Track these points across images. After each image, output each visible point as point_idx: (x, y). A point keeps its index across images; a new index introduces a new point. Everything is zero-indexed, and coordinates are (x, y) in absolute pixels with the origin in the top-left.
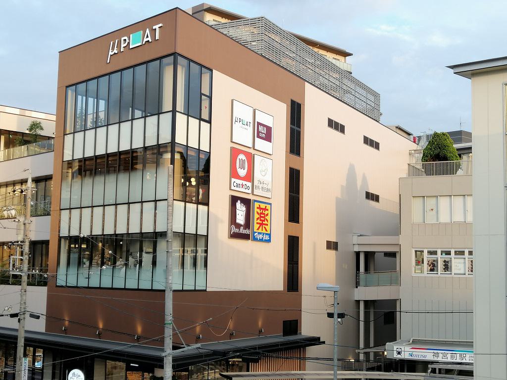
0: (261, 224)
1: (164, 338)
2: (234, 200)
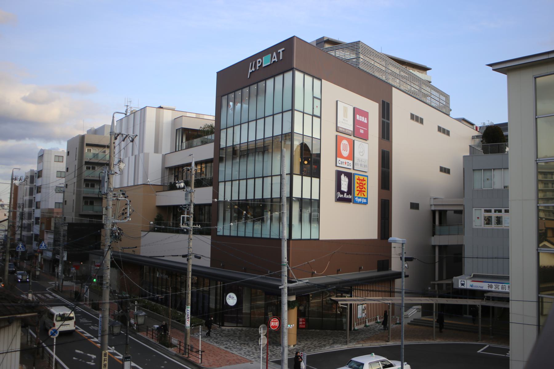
0: (360, 191)
1: (281, 272)
2: (339, 174)
